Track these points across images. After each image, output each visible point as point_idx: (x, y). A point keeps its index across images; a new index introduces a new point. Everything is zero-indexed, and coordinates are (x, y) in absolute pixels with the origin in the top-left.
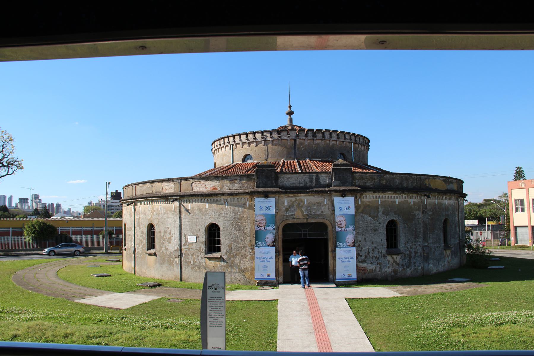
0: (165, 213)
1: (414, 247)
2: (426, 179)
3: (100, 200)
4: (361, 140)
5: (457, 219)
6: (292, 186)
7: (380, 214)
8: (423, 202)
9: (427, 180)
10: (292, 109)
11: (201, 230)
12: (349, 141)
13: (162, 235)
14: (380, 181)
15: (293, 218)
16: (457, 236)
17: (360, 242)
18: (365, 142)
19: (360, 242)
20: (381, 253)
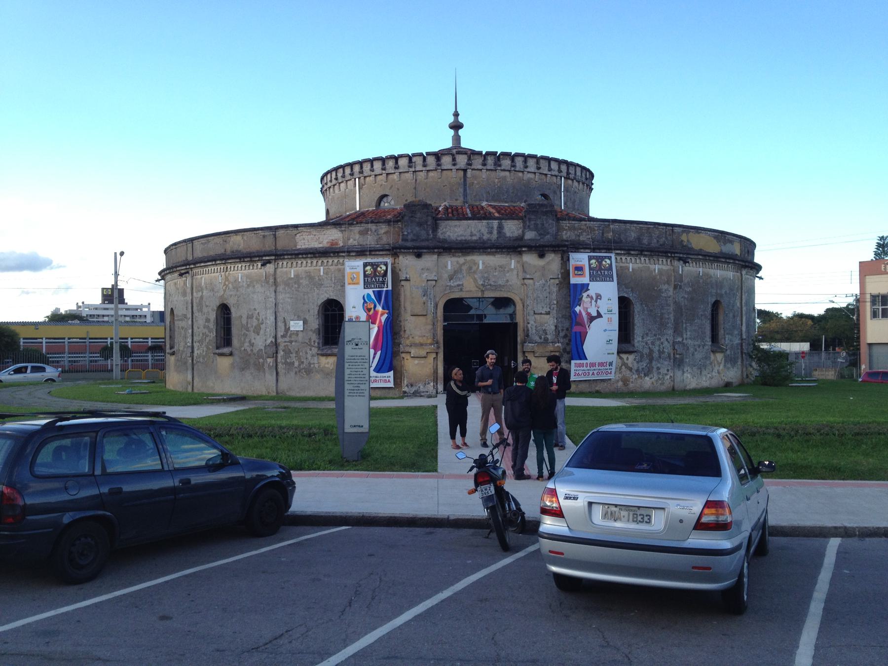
0: (248, 286)
1: (658, 343)
2: (683, 232)
3: (80, 304)
4: (579, 173)
5: (738, 304)
6: (459, 239)
8: (675, 271)
9: (685, 235)
11: (312, 311)
12: (557, 173)
13: (244, 322)
14: (603, 234)
15: (461, 290)
16: (736, 332)
18: (585, 177)
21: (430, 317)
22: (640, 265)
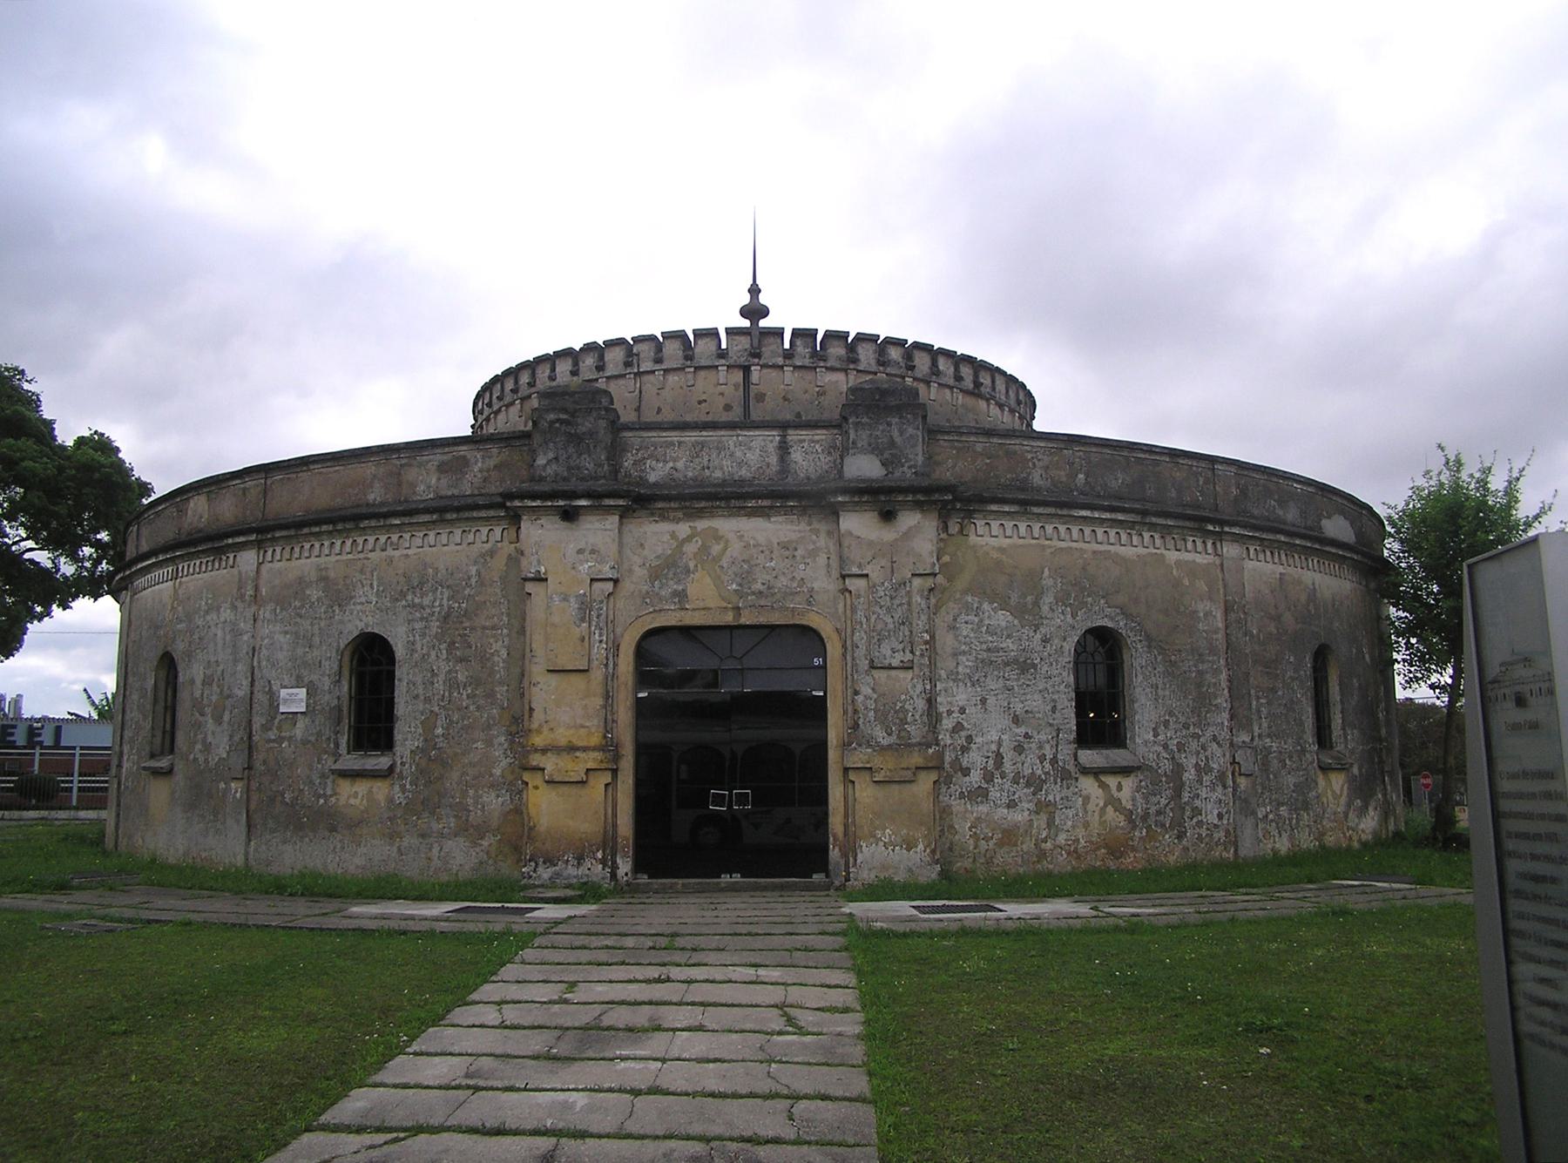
7: (1048, 599)
10: (763, 299)
11: (326, 664)
13: (197, 694)
17: (962, 711)
19: (962, 711)
20: (1054, 761)
21: (598, 674)
22: (1141, 550)
